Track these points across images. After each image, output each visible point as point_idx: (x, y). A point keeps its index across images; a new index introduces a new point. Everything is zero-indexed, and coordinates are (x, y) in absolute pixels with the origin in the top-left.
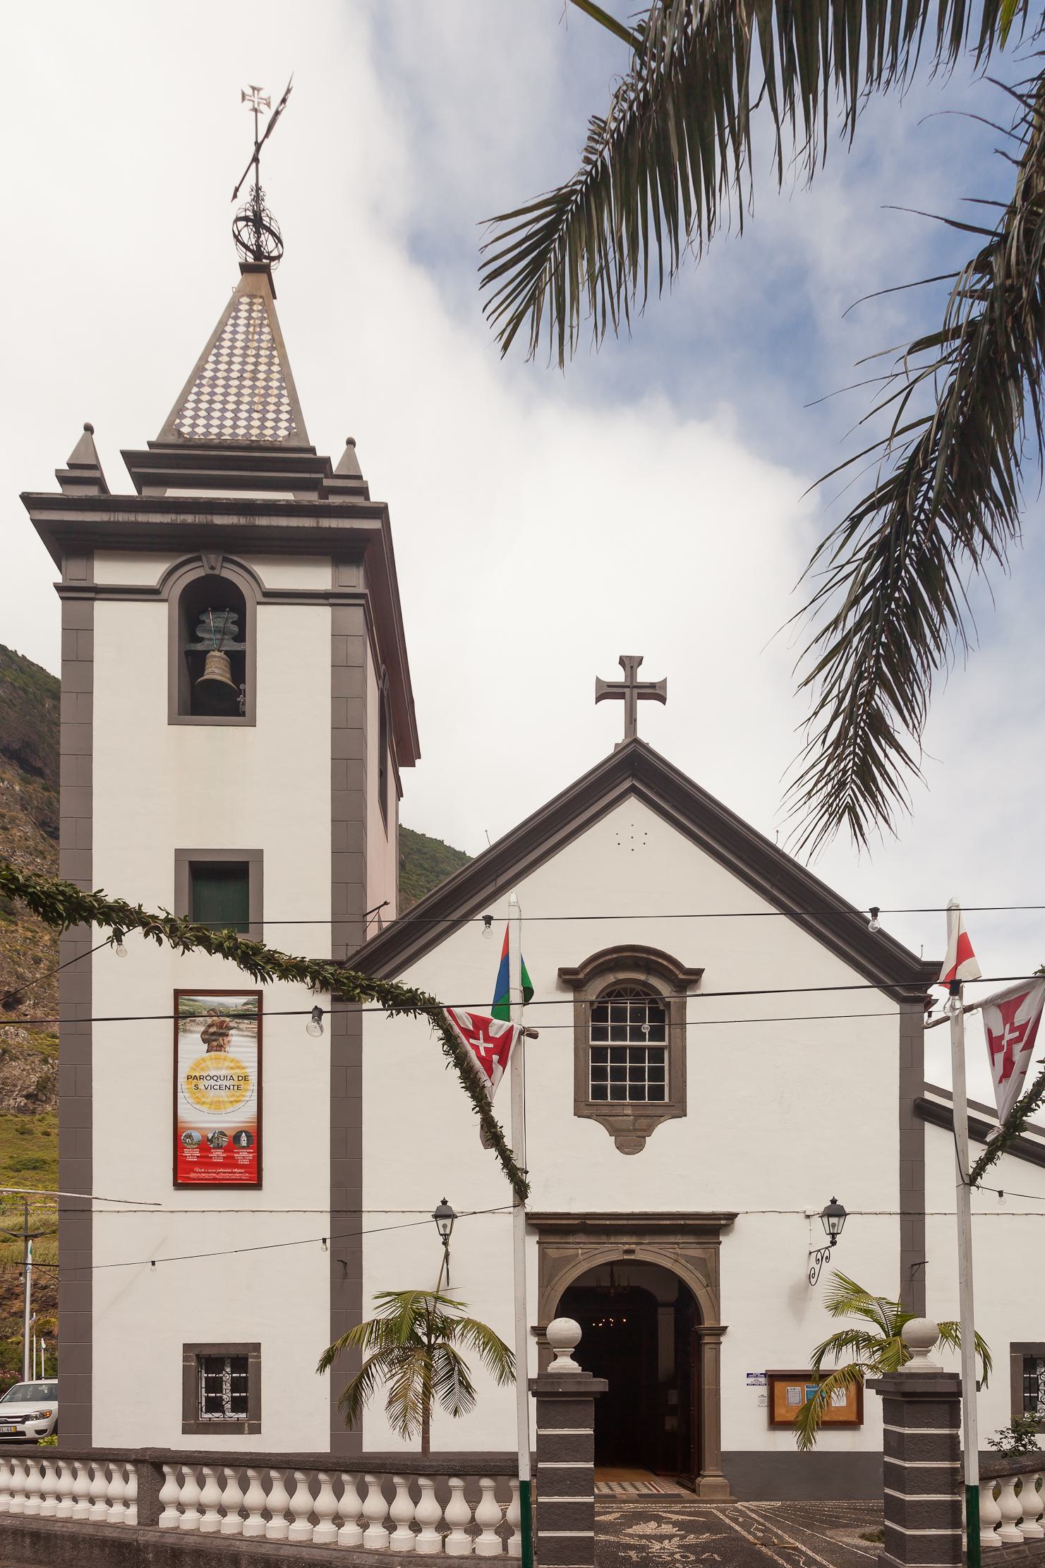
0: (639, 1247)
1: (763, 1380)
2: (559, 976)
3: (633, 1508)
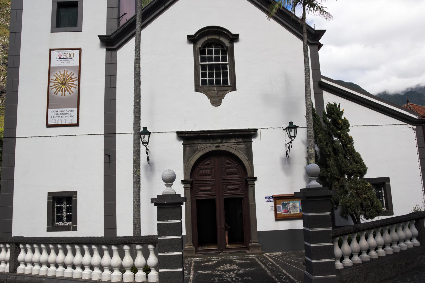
0: (221, 145)
1: (272, 199)
2: (188, 38)
3: (223, 258)
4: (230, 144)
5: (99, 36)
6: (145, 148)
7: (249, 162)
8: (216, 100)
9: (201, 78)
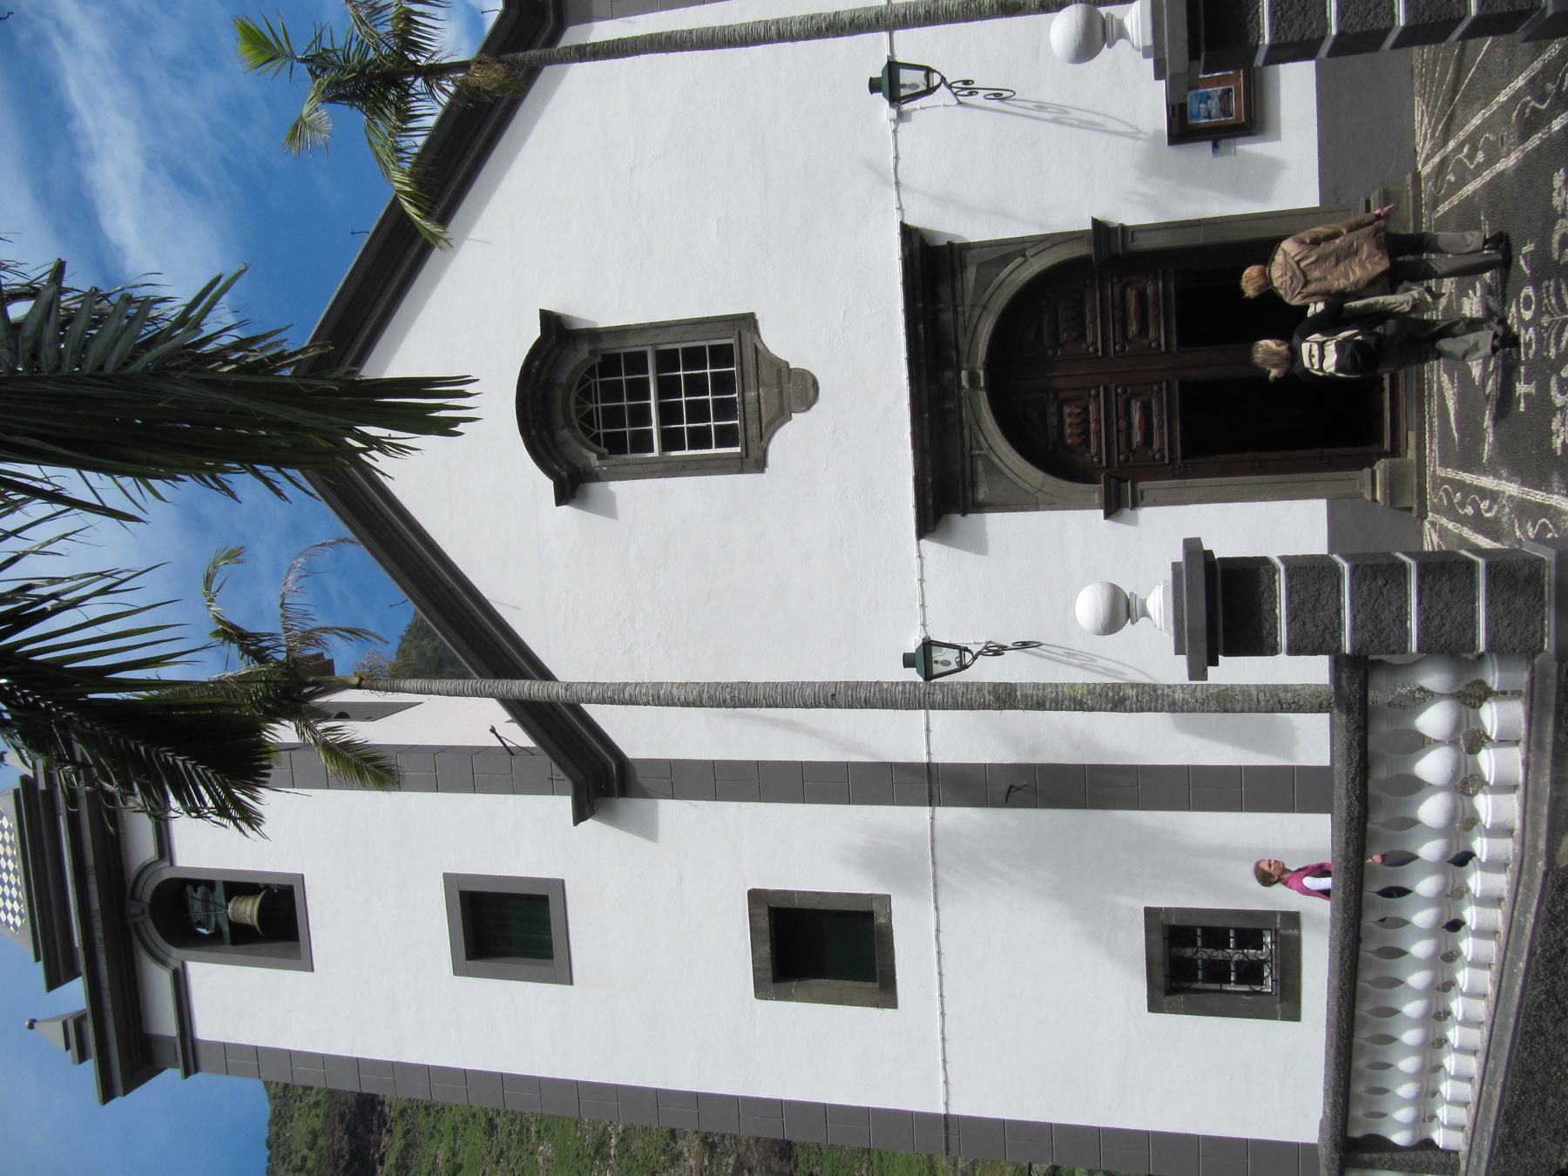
4: (960, 331)
5: (576, 822)
6: (980, 656)
7: (1032, 251)
8: (791, 392)
9: (710, 447)
